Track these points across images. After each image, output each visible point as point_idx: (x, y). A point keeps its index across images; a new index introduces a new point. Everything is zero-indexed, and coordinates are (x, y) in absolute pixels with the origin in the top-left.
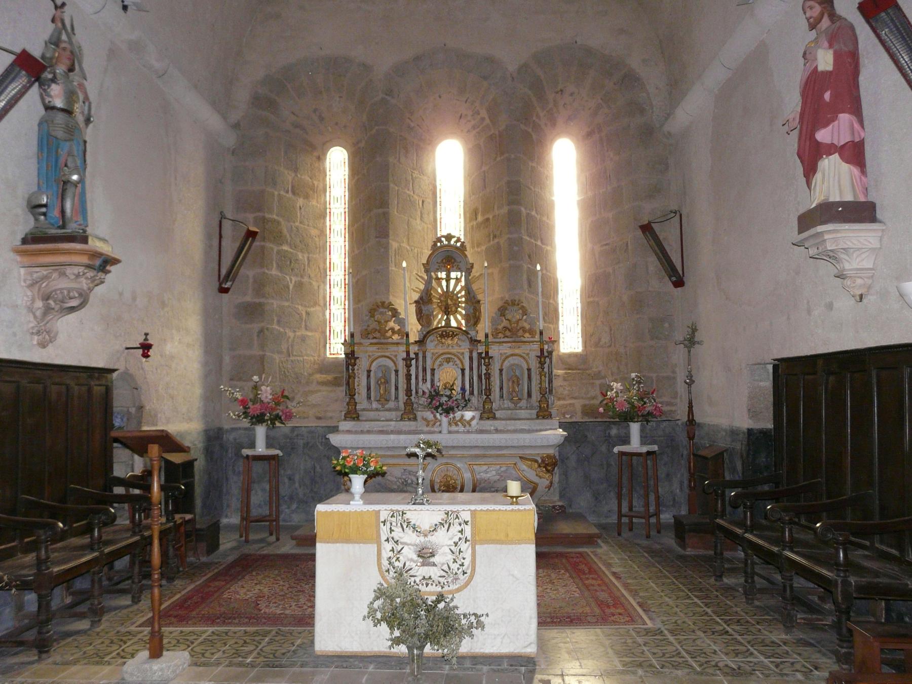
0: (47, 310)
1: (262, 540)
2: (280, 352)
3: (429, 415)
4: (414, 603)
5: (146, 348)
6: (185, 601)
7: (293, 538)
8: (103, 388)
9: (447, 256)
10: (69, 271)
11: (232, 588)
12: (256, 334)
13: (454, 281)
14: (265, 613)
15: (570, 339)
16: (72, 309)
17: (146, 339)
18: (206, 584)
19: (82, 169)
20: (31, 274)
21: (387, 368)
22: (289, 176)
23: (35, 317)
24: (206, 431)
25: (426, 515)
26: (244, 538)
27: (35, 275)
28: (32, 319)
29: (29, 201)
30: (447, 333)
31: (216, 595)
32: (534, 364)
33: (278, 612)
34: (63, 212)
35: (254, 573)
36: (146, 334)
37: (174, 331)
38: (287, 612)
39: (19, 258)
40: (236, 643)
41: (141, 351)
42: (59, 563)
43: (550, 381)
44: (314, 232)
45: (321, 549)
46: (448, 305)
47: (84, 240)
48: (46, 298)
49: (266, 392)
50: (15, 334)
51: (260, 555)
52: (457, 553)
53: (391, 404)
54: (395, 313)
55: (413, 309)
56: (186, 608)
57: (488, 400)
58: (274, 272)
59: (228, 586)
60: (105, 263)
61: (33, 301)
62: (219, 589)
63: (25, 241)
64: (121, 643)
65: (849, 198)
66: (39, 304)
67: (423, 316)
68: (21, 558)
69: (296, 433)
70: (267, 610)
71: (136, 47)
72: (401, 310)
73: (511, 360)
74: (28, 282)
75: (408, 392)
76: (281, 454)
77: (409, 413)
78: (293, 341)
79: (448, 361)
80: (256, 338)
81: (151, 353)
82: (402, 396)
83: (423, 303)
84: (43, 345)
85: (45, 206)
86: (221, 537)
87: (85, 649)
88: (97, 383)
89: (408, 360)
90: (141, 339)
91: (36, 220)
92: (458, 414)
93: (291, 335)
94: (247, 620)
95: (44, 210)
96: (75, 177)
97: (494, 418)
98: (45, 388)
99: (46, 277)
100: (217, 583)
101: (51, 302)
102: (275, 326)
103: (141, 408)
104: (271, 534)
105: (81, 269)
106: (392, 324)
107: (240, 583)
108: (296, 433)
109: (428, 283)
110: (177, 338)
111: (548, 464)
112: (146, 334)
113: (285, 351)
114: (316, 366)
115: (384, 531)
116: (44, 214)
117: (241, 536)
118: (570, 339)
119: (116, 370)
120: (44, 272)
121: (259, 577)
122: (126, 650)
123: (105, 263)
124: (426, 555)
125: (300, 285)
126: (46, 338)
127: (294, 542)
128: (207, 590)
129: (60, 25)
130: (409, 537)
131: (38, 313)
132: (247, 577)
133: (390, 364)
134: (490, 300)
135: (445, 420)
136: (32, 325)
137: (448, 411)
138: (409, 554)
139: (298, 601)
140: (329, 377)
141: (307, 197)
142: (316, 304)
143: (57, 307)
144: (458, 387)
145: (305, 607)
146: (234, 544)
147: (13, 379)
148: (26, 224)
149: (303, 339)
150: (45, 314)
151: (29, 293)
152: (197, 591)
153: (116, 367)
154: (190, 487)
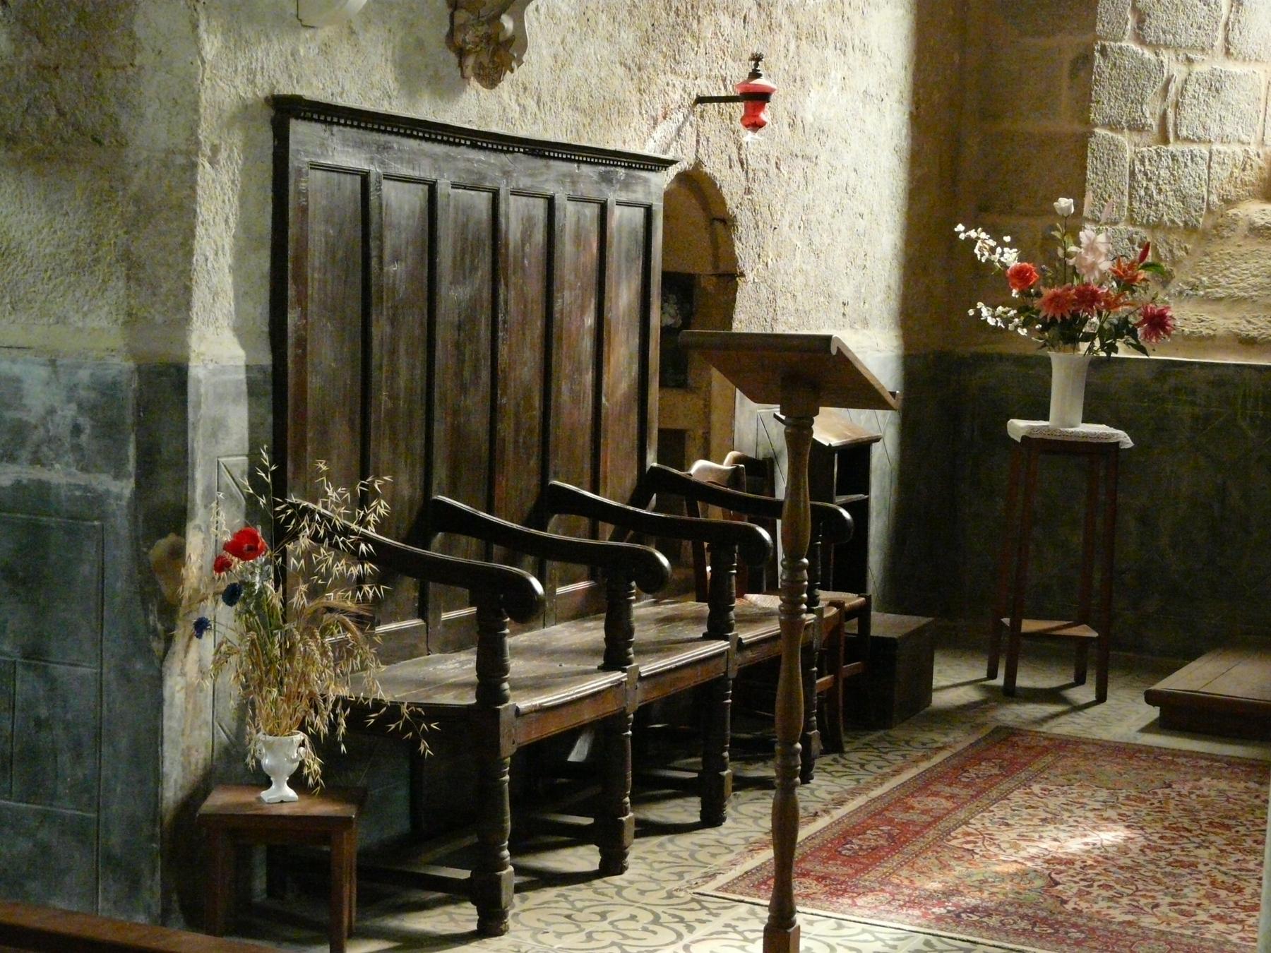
1: (1053, 696)
2: (1137, 127)
5: (756, 99)
6: (845, 837)
7: (1152, 698)
8: (639, 213)
11: (976, 823)
12: (1066, 67)
14: (1078, 912)
15: (1095, 634)
17: (755, 74)
18: (899, 799)
24: (139, 369)
26: (1000, 681)
31: (931, 834)
33: (1118, 915)
35: (1036, 788)
36: (757, 59)
37: (830, 53)
38: (1146, 921)
40: (642, 892)
41: (739, 109)
42: (538, 685)
49: (1092, 248)
51: (1051, 739)
56: (852, 859)
59: (962, 815)
62: (937, 819)
64: (681, 928)
68: (439, 661)
69: (1172, 381)
70: (1083, 905)
76: (1124, 438)
78: (1182, 92)
80: (1065, 83)
81: (765, 116)
86: (936, 669)
87: (588, 928)
88: (624, 197)
90: (737, 73)
93: (1177, 70)
94: (1024, 924)
100: (931, 802)
102: (1129, 44)
104: (1080, 680)
107: (998, 811)
108: (1172, 381)
110: (836, 75)
112: (757, 59)
113: (1153, 122)
114: (1250, 176)
117: (992, 674)
118: (1095, 634)
119: (672, 162)
121: (1053, 803)
122: (673, 937)
127: (1155, 712)
128: (900, 816)
132: (1017, 796)
139: (1177, 892)
145: (1202, 916)
146: (969, 695)
147: (416, 174)
152: (876, 813)
153: (669, 156)
154: (860, 511)
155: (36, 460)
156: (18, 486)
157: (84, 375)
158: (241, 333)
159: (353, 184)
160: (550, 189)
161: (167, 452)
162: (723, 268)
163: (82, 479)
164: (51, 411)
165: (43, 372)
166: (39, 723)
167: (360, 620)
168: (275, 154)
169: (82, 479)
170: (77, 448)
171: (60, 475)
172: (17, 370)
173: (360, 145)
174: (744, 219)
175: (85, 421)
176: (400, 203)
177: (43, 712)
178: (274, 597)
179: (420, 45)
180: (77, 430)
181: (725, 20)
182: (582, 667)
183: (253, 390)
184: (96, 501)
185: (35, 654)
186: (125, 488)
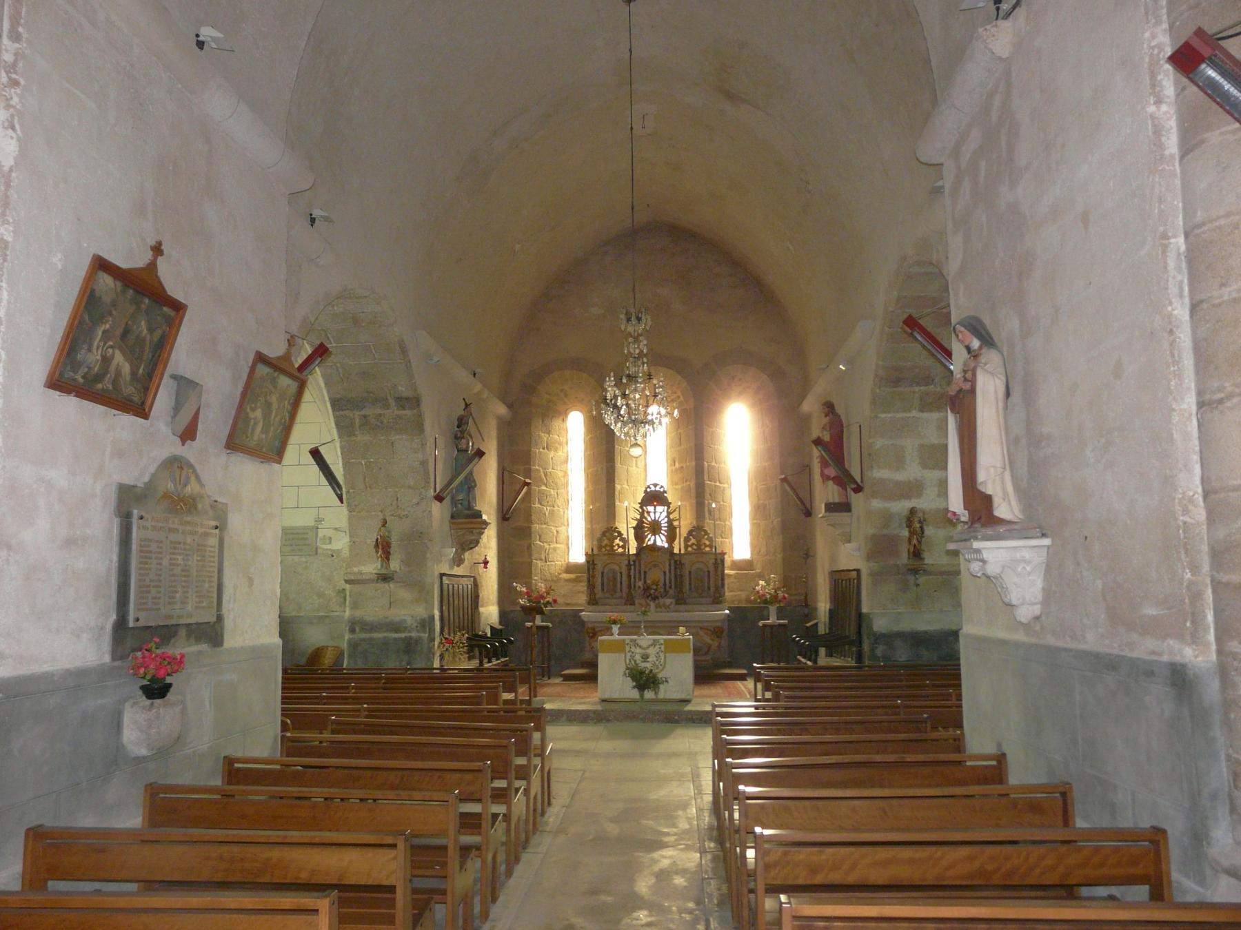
3: (643, 601)
4: (642, 673)
9: (654, 497)
13: (659, 513)
21: (614, 572)
22: (545, 437)
25: (646, 639)
30: (654, 548)
32: (712, 569)
43: (723, 580)
44: (561, 474)
45: (601, 656)
46: (655, 528)
52: (658, 656)
53: (618, 594)
54: (620, 534)
55: (632, 532)
57: (681, 591)
58: (537, 505)
65: (837, 500)
67: (639, 536)
72: (624, 532)
73: (698, 565)
75: (629, 586)
77: (630, 601)
79: (655, 566)
82: (625, 589)
83: (639, 531)
89: (629, 565)
92: (661, 601)
97: (685, 603)
106: (617, 541)
109: (642, 514)
111: (717, 632)
115: (627, 648)
124: (645, 657)
125: (552, 512)
130: (638, 650)
133: (617, 568)
134: (684, 526)
135: (652, 605)
137: (655, 598)
138: (638, 657)
140: (572, 576)
141: (556, 450)
142: (563, 524)
144: (661, 584)
149: (555, 549)
171: (414, 634)
184: (420, 638)
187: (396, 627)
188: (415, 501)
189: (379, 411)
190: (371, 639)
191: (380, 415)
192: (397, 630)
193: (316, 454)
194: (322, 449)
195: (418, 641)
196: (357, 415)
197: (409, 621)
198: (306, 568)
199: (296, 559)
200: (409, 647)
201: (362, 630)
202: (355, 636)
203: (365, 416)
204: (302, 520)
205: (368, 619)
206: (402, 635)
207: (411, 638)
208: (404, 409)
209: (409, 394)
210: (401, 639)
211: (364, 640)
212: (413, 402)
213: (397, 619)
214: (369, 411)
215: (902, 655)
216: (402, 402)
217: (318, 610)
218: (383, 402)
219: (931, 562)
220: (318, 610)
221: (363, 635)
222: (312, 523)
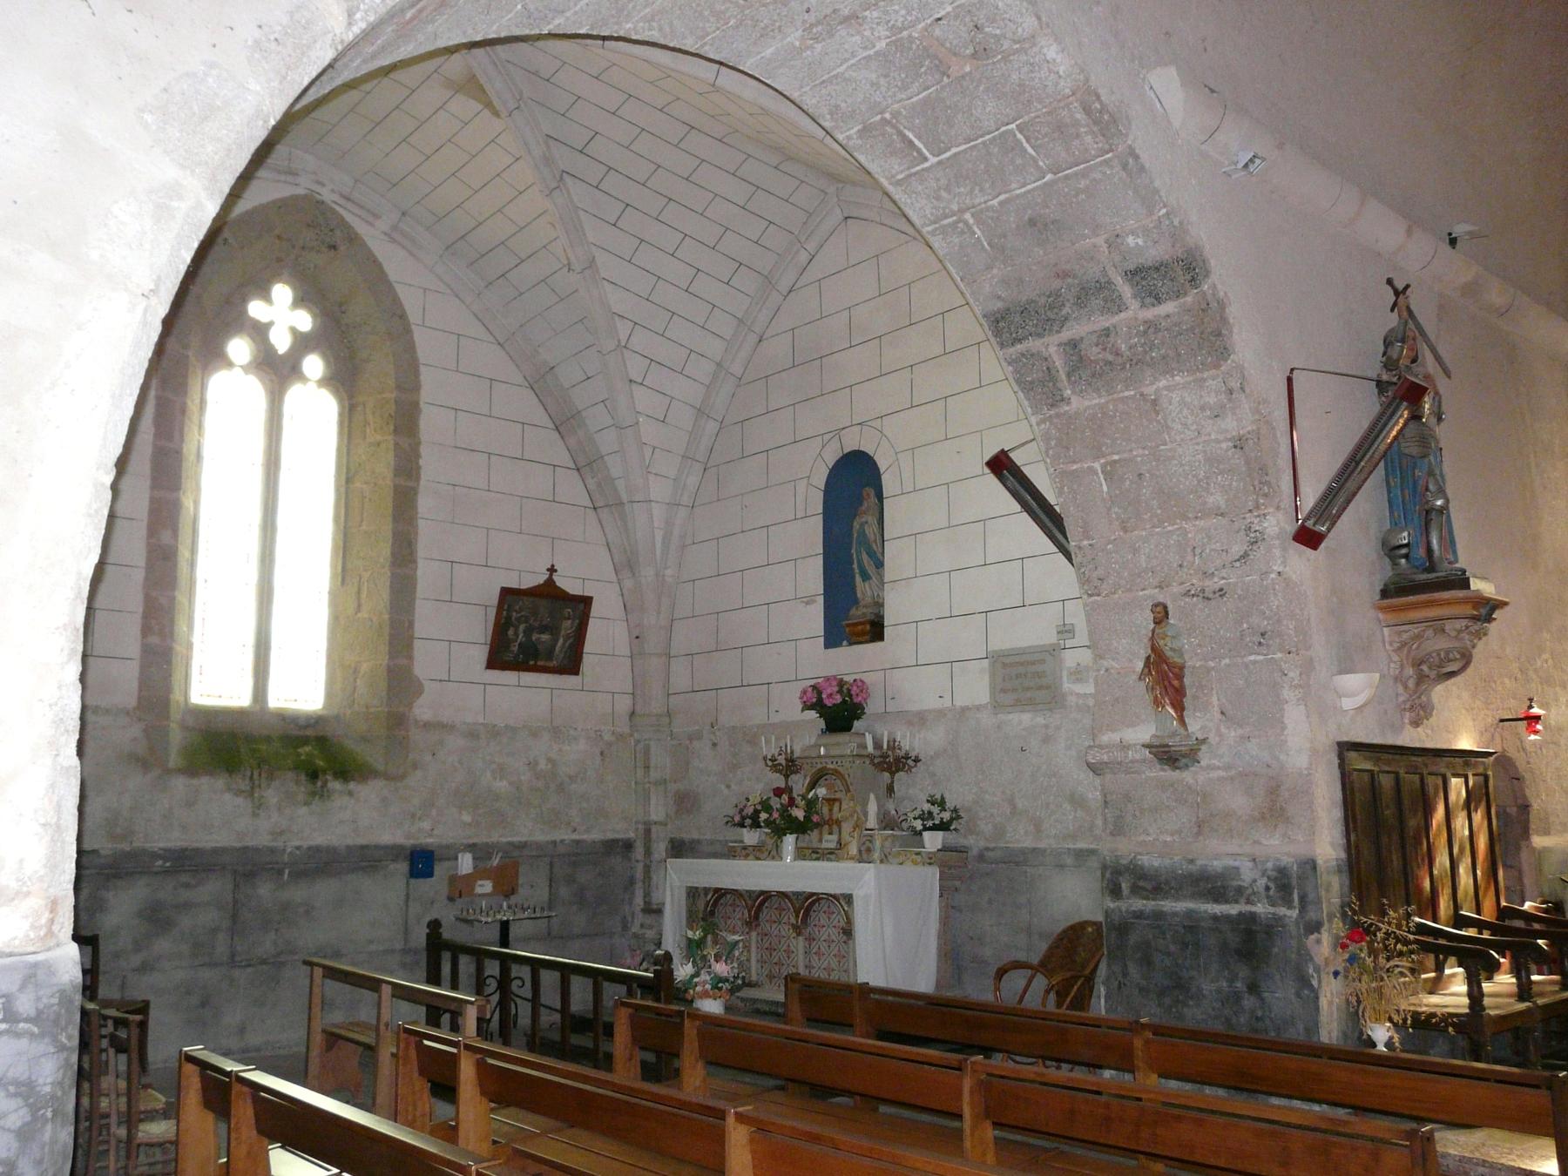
0: (1421, 678)
10: (1449, 626)
15: (872, 796)
16: (1452, 674)
19: (1441, 492)
20: (1399, 633)
23: (1406, 687)
27: (1405, 636)
28: (1401, 689)
29: (1384, 544)
34: (1429, 551)
39: (1381, 616)
47: (1465, 584)
48: (1418, 664)
50: (1386, 712)
60: (1487, 609)
61: (1402, 666)
63: (1385, 593)
66: (1410, 671)
71: (1471, 290)
74: (1396, 645)
84: (1416, 723)
85: (1407, 545)
91: (1395, 564)
95: (1404, 551)
96: (1439, 503)
98: (1422, 780)
99: (1418, 637)
101: (1425, 668)
103: (1525, 808)
105: (1464, 623)
116: (1406, 556)
118: (872, 796)
120: (1415, 630)
123: (1487, 609)
126: (1420, 712)
129: (1405, 314)
131: (1411, 684)
136: (1401, 699)
143: (1433, 674)
148: (1383, 572)
150: (1418, 684)
151: (1396, 658)
155: (1248, 902)
156: (1240, 914)
157: (1270, 865)
158: (1332, 844)
159: (1366, 777)
160: (1443, 770)
161: (1311, 896)
162: (1520, 801)
163: (1272, 910)
164: (1255, 881)
165: (1250, 865)
166: (1257, 1019)
167: (1413, 971)
168: (275, 128)
169: (1272, 910)
170: (1268, 897)
171: (1261, 908)
172: (1237, 864)
173: (1369, 759)
174: (1527, 776)
175: (1272, 885)
176: (1386, 781)
177: (1260, 1014)
178: (1369, 961)
179: (1386, 712)
180: (1267, 888)
181: (1507, 681)
182: (816, 1129)
183: (1340, 871)
184: (1279, 919)
185: (1253, 988)
186: (1294, 913)
187: (1214, 886)
188: (1237, 549)
189: (1105, 321)
190: (1159, 915)
191: (1106, 332)
192: (1219, 895)
193: (1001, 465)
194: (1017, 457)
195: (1272, 928)
196: (1050, 346)
197: (1248, 873)
198: (1046, 740)
199: (1026, 718)
200: (1251, 944)
201: (1136, 890)
202: (1123, 905)
203: (1074, 344)
204: (1033, 632)
205: (1150, 861)
206: (1233, 910)
207: (1253, 917)
208: (1159, 300)
209: (1157, 252)
210: (1227, 918)
211: (1139, 915)
212: (1179, 271)
213: (1217, 865)
214: (1080, 328)
215: (1413, 823)
216: (1151, 279)
217: (1074, 837)
218: (1095, 292)
219: (1335, 1034)
220: (1074, 837)
221: (1138, 904)
222: (1050, 638)
